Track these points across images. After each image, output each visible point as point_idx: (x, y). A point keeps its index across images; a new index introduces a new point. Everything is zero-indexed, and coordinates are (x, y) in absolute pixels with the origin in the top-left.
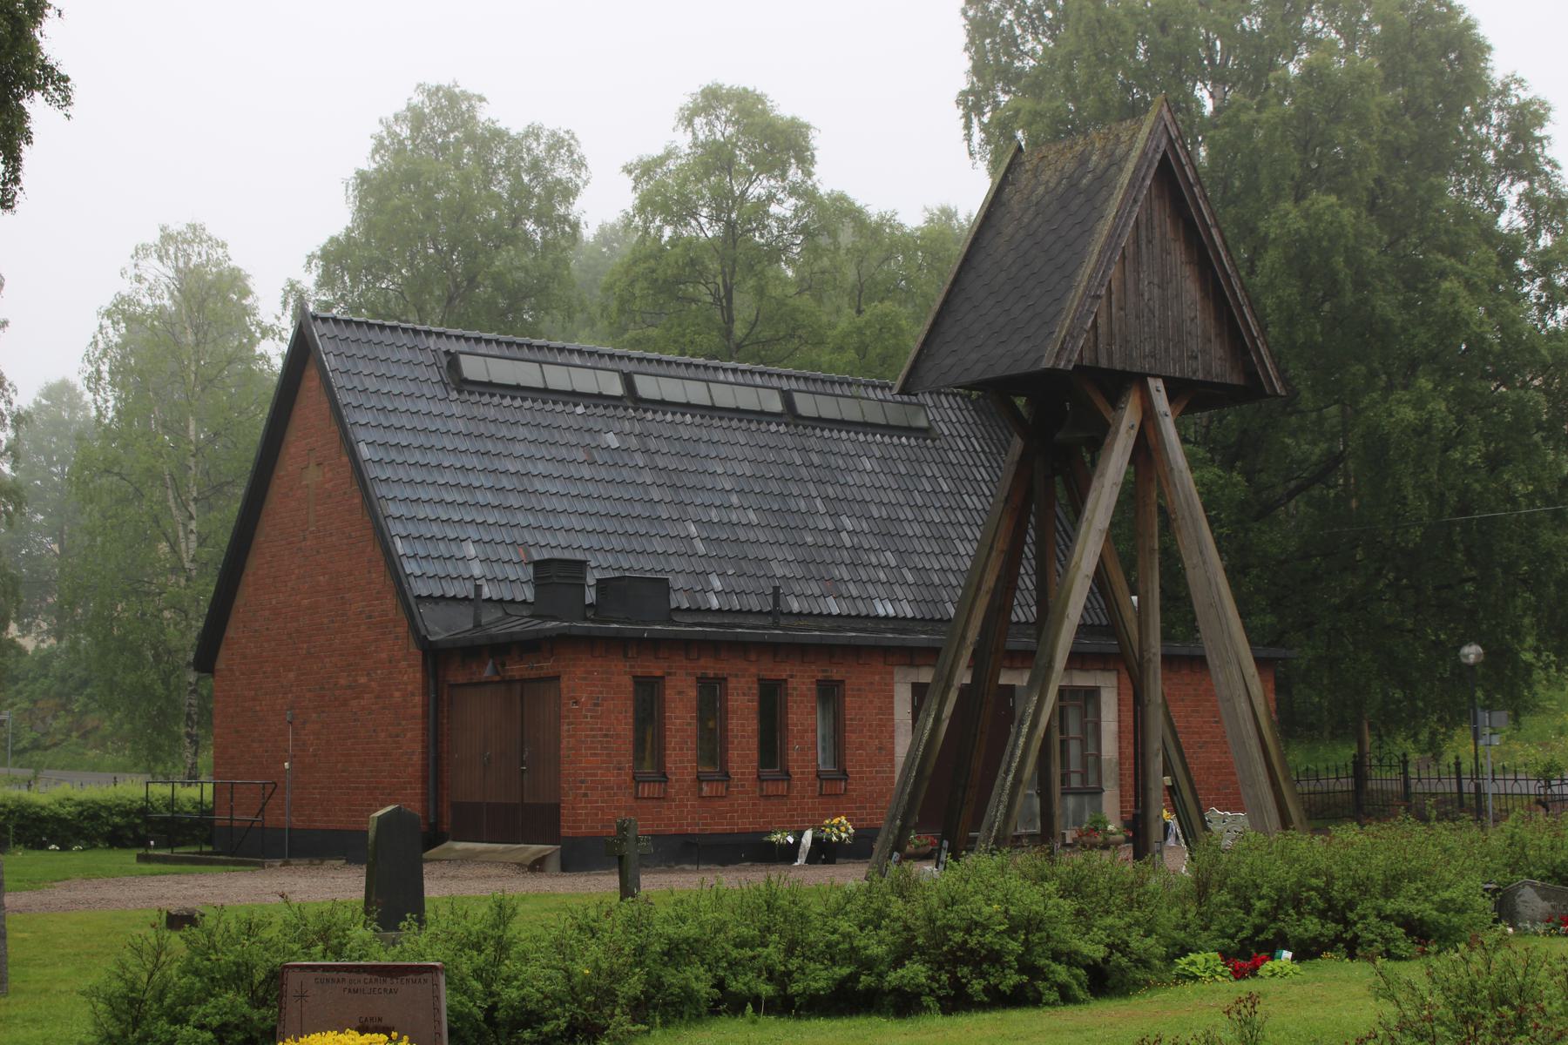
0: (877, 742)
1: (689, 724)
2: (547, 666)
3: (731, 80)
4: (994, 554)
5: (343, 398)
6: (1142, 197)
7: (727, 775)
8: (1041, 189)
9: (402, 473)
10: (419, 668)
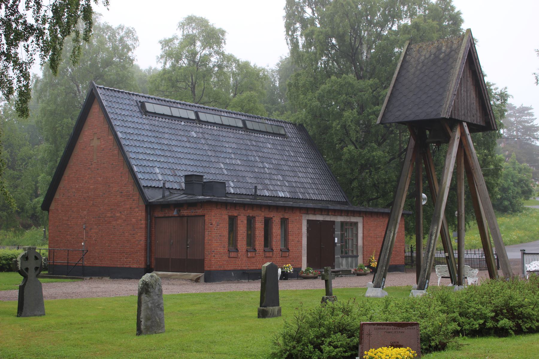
0: (297, 239)
1: (244, 232)
2: (200, 212)
3: (198, 14)
4: (408, 179)
5: (111, 116)
6: (465, 62)
7: (255, 249)
8: (423, 58)
9: (132, 143)
10: (144, 211)
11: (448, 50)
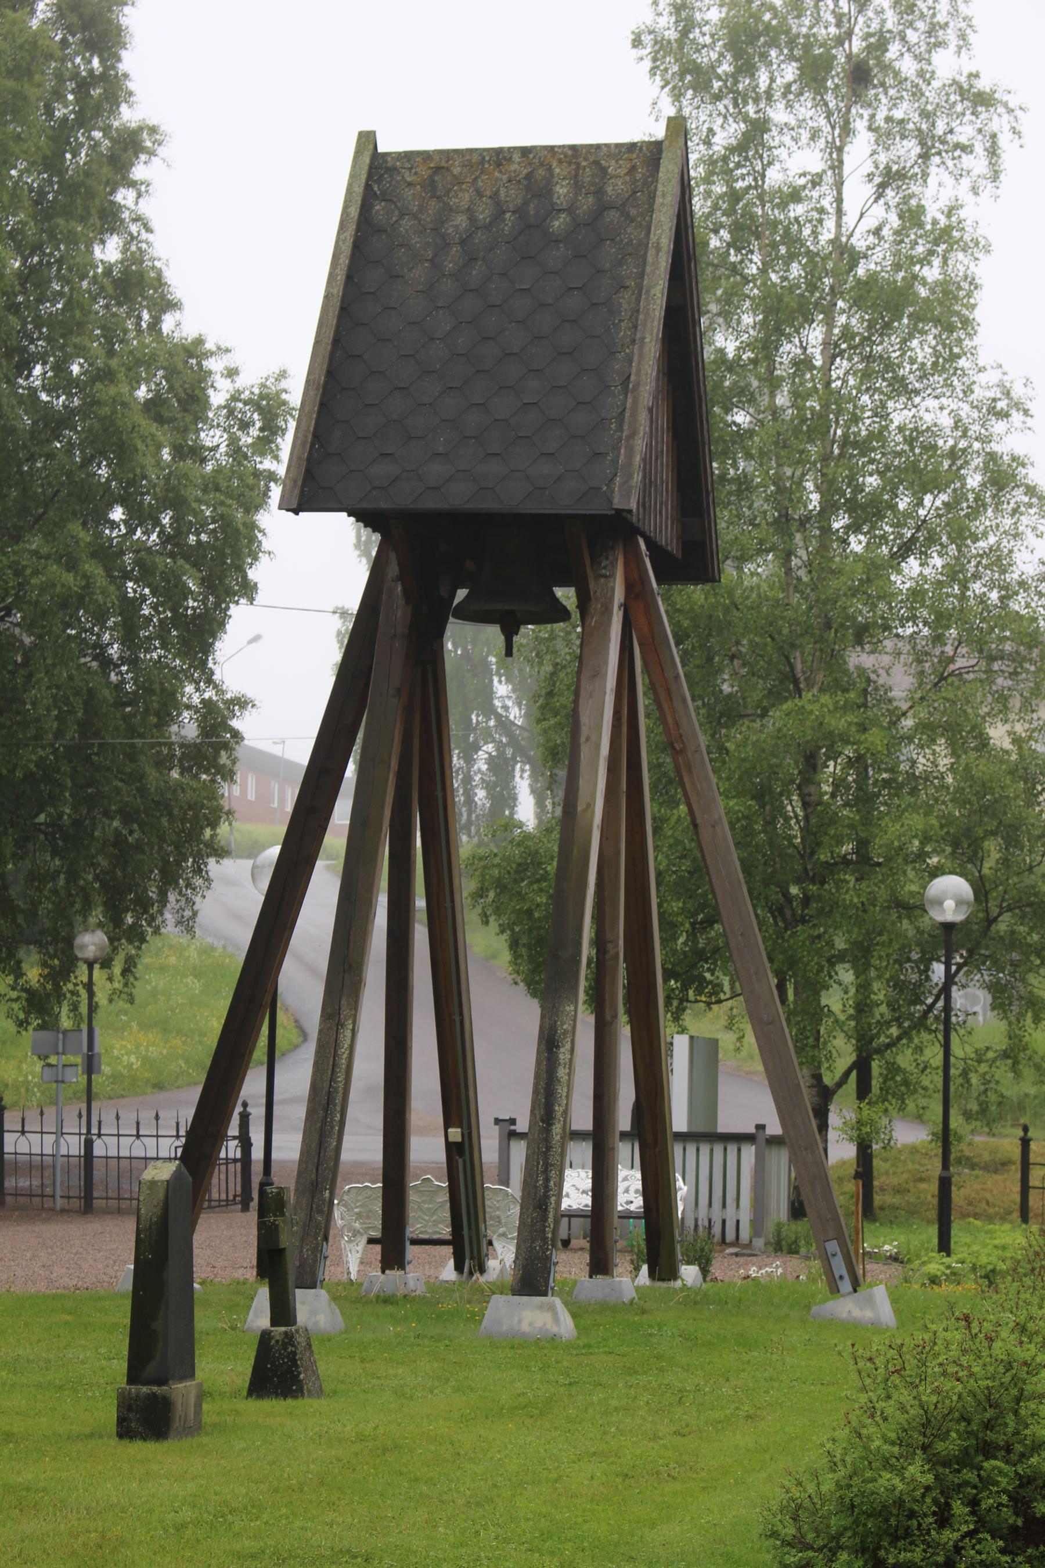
8: (461, 221)
11: (587, 203)
